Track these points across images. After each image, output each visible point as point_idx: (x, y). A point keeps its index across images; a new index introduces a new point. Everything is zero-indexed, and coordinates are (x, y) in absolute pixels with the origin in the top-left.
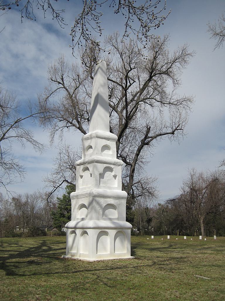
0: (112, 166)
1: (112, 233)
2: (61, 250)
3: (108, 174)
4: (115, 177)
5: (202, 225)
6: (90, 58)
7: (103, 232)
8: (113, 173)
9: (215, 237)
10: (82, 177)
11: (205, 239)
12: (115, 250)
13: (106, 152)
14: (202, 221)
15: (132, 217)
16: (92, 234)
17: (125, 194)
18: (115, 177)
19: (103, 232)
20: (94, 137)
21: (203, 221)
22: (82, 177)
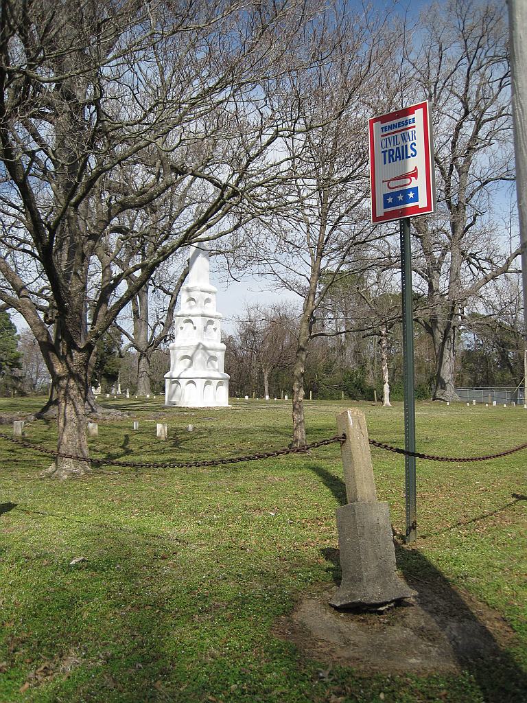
0: (214, 319)
3: (211, 327)
4: (215, 329)
7: (208, 381)
8: (214, 326)
9: (267, 397)
10: (182, 328)
11: (154, 397)
12: (219, 397)
14: (266, 377)
16: (200, 383)
17: (224, 346)
18: (215, 329)
19: (208, 381)
22: (182, 328)
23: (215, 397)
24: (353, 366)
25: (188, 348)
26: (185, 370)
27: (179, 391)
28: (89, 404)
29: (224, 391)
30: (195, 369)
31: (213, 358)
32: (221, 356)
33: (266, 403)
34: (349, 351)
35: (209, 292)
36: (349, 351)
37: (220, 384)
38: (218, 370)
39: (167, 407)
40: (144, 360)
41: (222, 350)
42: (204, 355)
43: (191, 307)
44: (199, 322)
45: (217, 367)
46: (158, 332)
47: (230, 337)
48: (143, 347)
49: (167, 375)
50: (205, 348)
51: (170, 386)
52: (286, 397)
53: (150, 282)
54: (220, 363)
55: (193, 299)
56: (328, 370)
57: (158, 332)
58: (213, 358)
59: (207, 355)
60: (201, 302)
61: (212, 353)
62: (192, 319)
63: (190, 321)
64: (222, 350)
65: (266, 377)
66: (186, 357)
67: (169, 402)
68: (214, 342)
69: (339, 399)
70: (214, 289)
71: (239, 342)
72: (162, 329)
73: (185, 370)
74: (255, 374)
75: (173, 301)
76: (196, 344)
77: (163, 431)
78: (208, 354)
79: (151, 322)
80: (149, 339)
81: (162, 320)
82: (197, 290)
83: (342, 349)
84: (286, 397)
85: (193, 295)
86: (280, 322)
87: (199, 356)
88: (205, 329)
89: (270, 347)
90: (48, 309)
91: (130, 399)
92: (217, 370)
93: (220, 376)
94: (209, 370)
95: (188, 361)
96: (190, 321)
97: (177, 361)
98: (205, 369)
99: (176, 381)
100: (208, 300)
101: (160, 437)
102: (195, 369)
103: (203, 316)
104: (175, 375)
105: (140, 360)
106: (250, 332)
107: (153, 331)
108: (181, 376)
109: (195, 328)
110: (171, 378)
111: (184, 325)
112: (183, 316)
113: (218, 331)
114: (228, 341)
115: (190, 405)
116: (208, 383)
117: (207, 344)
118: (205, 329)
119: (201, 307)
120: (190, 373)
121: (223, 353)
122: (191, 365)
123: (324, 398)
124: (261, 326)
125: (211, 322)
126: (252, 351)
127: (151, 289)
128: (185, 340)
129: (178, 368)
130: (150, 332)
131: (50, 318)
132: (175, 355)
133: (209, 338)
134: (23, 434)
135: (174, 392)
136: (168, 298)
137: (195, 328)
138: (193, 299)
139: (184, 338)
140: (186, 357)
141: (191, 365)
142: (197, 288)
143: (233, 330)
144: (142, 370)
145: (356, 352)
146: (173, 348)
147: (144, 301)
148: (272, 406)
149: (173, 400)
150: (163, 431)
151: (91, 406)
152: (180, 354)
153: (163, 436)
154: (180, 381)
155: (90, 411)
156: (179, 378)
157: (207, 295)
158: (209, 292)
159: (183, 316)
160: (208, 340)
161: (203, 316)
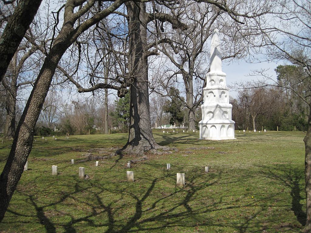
0: (225, 91)
1: (227, 126)
2: (186, 135)
3: (223, 95)
4: (226, 96)
5: (254, 123)
6: (192, 19)
7: (223, 125)
8: (225, 95)
9: (255, 131)
10: (207, 96)
11: (197, 132)
12: (228, 134)
13: (221, 83)
14: (254, 120)
15: (182, 116)
16: (218, 127)
17: (231, 105)
18: (226, 96)
19: (223, 125)
20: (215, 75)
21: (255, 120)
22: (207, 96)
23: (227, 134)
24: (298, 113)
25: (211, 107)
26: (210, 119)
27: (207, 132)
28: (150, 144)
29: (232, 131)
30: (215, 119)
31: (226, 112)
32: (230, 111)
33: (254, 134)
34: (294, 105)
35: (222, 76)
36: (294, 105)
37: (229, 126)
38: (228, 119)
39: (200, 140)
40: (191, 113)
41: (230, 108)
42: (220, 111)
43: (212, 85)
44: (216, 92)
45: (227, 117)
46: (198, 98)
47: (235, 100)
48: (191, 107)
49: (200, 122)
50: (220, 107)
51: (202, 129)
52: (265, 130)
53: (194, 74)
54: (229, 115)
55: (213, 80)
56: (285, 115)
57: (198, 98)
58: (226, 112)
59: (221, 111)
60: (217, 82)
61: (224, 110)
62: (213, 91)
63: (212, 92)
64: (230, 108)
65: (254, 120)
66: (210, 112)
67: (202, 137)
68: (226, 103)
69: (292, 130)
70: (225, 74)
71: (239, 102)
72: (200, 97)
73: (210, 119)
74: (248, 118)
75: (205, 83)
76: (215, 105)
77: (181, 180)
78: (222, 110)
79: (195, 94)
80: (194, 102)
81: (200, 93)
82: (215, 75)
83: (291, 104)
84: (265, 130)
85: (213, 78)
86: (260, 91)
87: (217, 112)
88: (220, 96)
89: (255, 103)
90: (120, 88)
91: (184, 133)
92: (228, 119)
93: (229, 122)
94: (223, 119)
95: (211, 114)
96: (212, 92)
97: (205, 115)
98: (220, 119)
99: (205, 125)
100: (221, 80)
101: (179, 184)
102: (215, 119)
103: (219, 89)
104: (204, 122)
105: (189, 113)
106: (244, 97)
107: (196, 99)
108: (208, 123)
109: (215, 96)
110: (202, 124)
111: (209, 95)
112: (208, 90)
113: (228, 97)
114: (233, 102)
115: (213, 139)
116: (223, 126)
117: (221, 105)
118: (220, 96)
119: (217, 84)
120: (213, 121)
121: (231, 109)
122: (213, 117)
123: (284, 129)
124: (250, 93)
125: (223, 93)
126: (246, 106)
127: (194, 78)
128: (209, 103)
129: (206, 119)
130: (194, 99)
131: (121, 94)
132: (204, 112)
133: (223, 101)
134: (85, 176)
135: (204, 132)
136: (203, 81)
137: (215, 96)
138: (213, 80)
139: (209, 102)
140: (210, 112)
141: (213, 117)
142: (215, 74)
143: (236, 95)
144: (191, 118)
145: (298, 105)
146: (203, 108)
147: (191, 84)
148: (259, 137)
149: (204, 136)
150: (181, 180)
151: (151, 145)
152: (206, 111)
153: (181, 183)
154: (208, 125)
155: (150, 148)
156: (207, 124)
157: (221, 78)
158: (222, 76)
159: (208, 90)
160: (222, 102)
161: (219, 89)
